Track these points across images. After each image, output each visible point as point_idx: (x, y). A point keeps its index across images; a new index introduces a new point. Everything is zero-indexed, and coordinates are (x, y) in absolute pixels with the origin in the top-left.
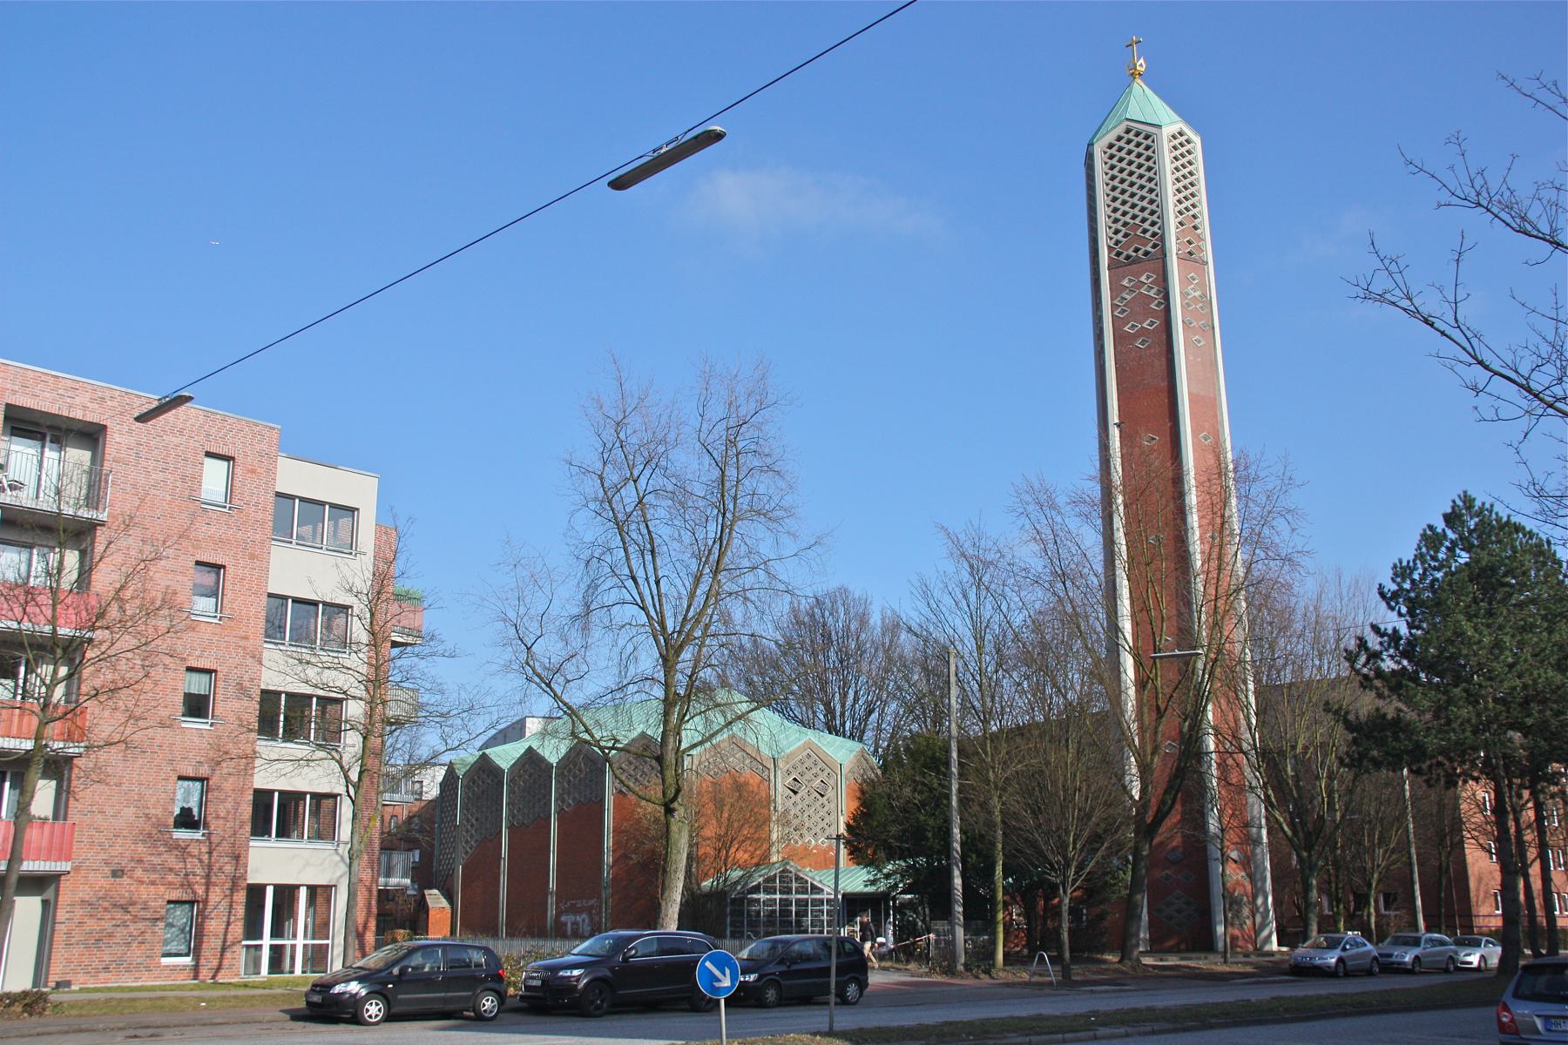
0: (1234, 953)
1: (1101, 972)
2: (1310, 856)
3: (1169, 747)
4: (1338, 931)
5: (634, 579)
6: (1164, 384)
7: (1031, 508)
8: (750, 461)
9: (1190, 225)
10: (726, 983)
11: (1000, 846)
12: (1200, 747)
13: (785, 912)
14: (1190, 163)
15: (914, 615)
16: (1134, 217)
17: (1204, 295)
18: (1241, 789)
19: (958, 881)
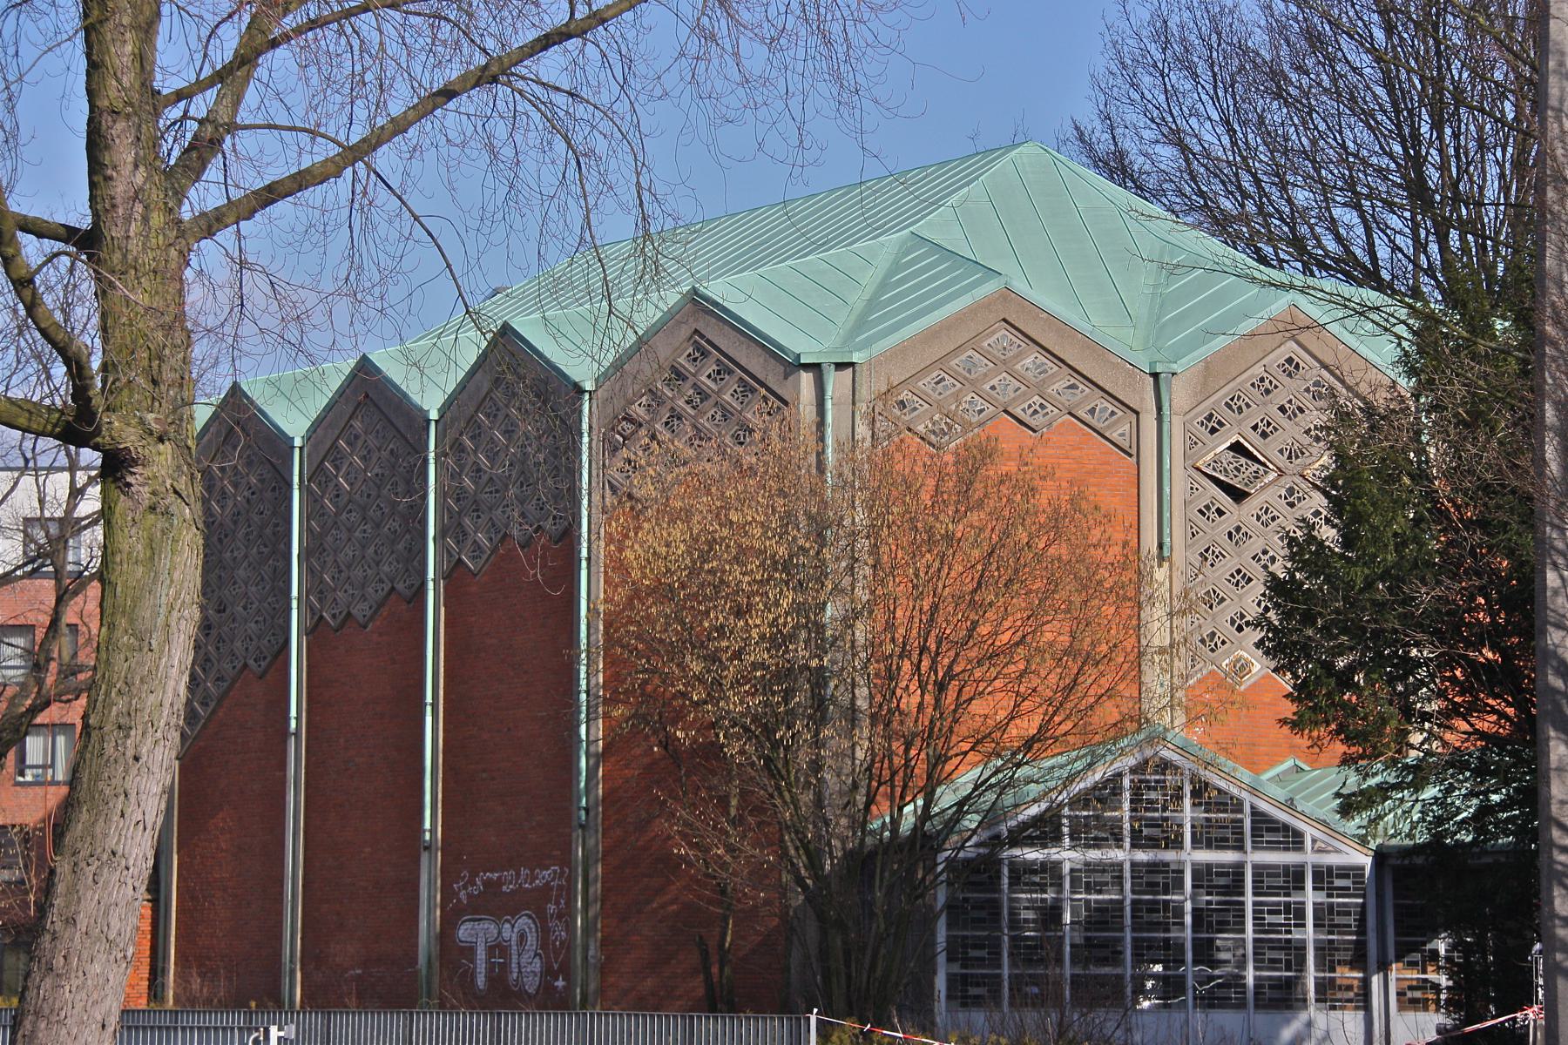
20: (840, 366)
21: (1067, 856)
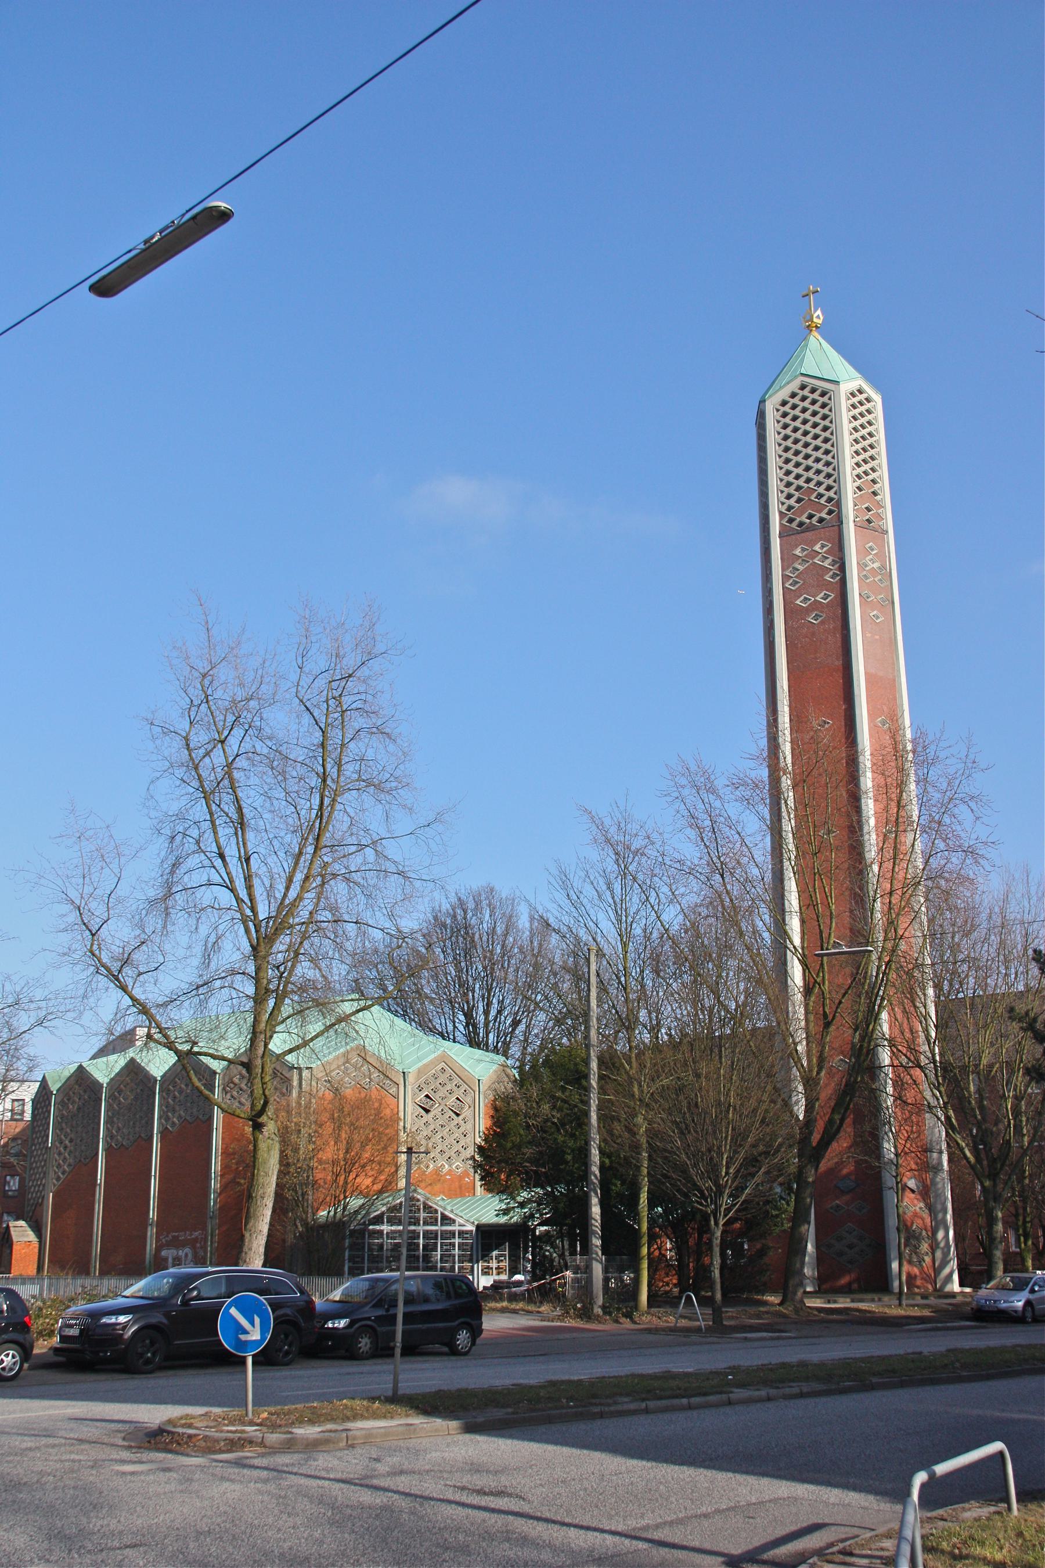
0: (911, 1294)
1: (758, 1316)
2: (995, 1185)
3: (838, 1061)
4: (1026, 1271)
5: (222, 856)
6: (839, 663)
7: (686, 792)
8: (358, 721)
9: (868, 491)
10: (255, 1336)
11: (645, 1171)
12: (872, 1062)
13: (412, 1247)
14: (870, 423)
15: (552, 906)
16: (808, 480)
17: (883, 567)
18: (920, 1108)
19: (596, 1210)
20: (307, 1068)
21: (385, 1228)
